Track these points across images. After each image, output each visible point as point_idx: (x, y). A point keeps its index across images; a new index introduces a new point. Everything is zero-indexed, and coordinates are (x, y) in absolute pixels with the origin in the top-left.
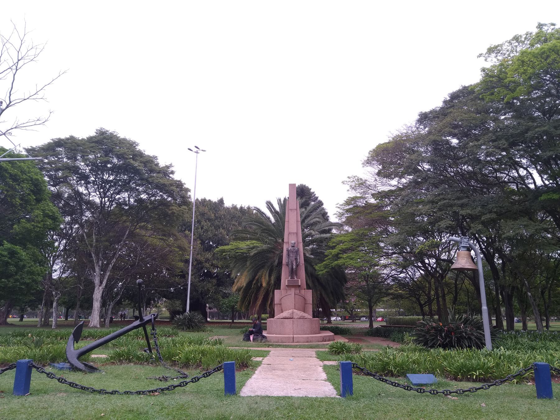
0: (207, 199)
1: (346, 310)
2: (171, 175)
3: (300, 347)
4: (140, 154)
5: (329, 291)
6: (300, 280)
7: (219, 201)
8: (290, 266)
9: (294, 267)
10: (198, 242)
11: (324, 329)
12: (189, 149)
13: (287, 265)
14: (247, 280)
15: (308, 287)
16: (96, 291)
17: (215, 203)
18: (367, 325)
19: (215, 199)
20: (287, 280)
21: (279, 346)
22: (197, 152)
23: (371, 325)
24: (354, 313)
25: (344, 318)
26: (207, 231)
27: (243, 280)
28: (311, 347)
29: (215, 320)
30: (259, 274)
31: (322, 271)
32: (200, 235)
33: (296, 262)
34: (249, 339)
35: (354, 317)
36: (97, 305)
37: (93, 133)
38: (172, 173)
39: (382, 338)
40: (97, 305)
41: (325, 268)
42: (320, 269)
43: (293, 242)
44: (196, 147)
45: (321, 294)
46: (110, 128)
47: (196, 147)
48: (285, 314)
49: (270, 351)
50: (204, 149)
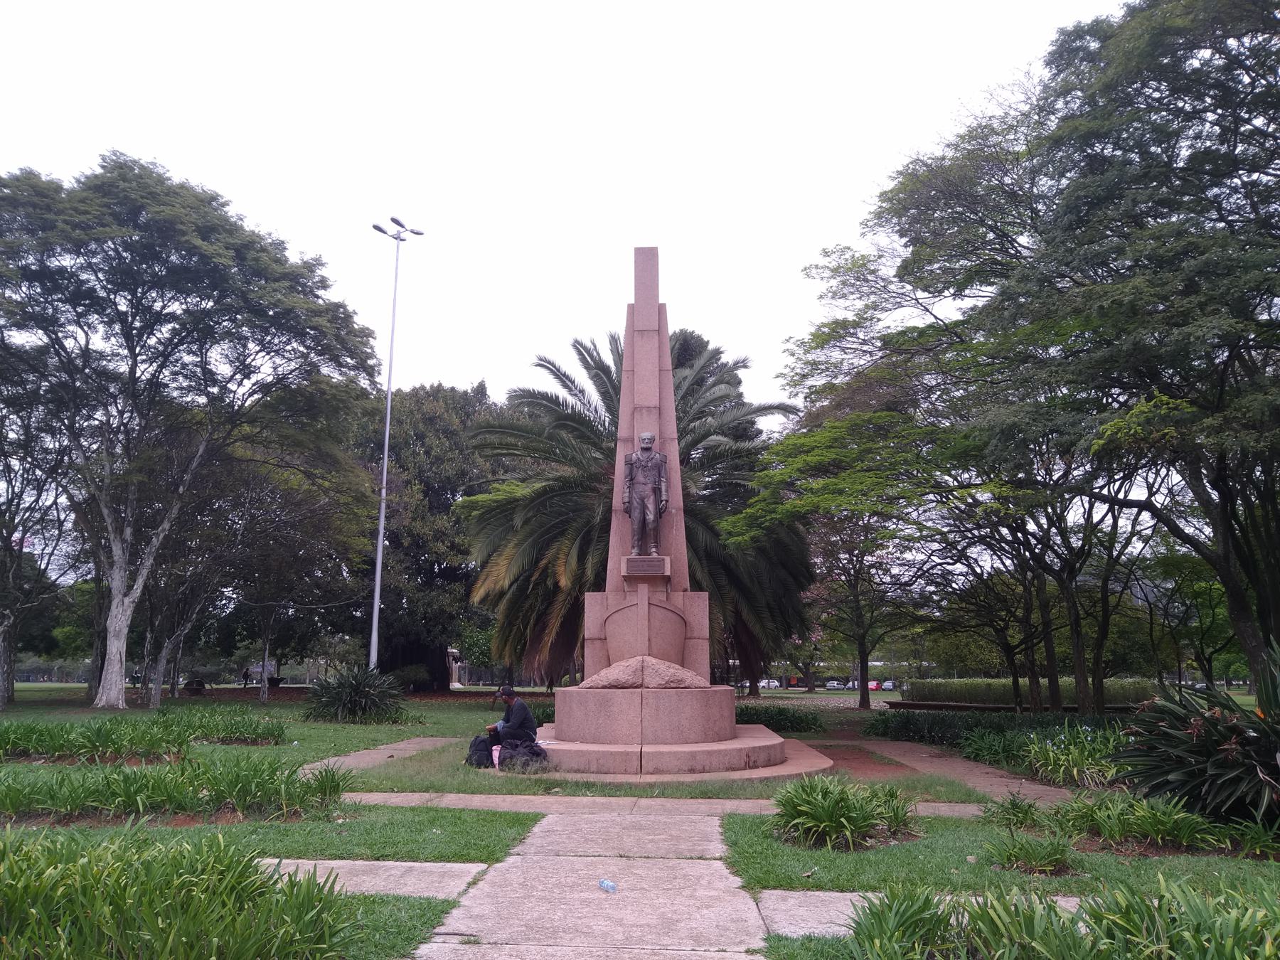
0: (447, 385)
1: (795, 664)
2: (320, 293)
3: (666, 791)
4: (232, 228)
5: (765, 588)
6: (667, 560)
7: (474, 390)
8: (636, 514)
9: (651, 517)
10: (415, 488)
11: (746, 717)
12: (377, 228)
13: (628, 511)
14: (515, 570)
15: (696, 586)
16: (114, 610)
17: (465, 393)
18: (853, 700)
19: (464, 384)
20: (624, 559)
21: (589, 787)
22: (397, 237)
23: (865, 702)
24: (812, 670)
25: (787, 683)
26: (439, 460)
27: (503, 569)
28: (706, 793)
29: (481, 688)
30: (550, 553)
31: (743, 534)
32: (421, 471)
33: (658, 501)
34: (486, 761)
35: (811, 680)
36: (116, 647)
37: (93, 167)
38: (324, 284)
39: (935, 750)
40: (116, 647)
41: (750, 526)
42: (734, 529)
43: (646, 435)
44: (395, 221)
45: (737, 613)
46: (141, 151)
47: (395, 221)
48: (617, 672)
49: (536, 818)
50: (417, 229)
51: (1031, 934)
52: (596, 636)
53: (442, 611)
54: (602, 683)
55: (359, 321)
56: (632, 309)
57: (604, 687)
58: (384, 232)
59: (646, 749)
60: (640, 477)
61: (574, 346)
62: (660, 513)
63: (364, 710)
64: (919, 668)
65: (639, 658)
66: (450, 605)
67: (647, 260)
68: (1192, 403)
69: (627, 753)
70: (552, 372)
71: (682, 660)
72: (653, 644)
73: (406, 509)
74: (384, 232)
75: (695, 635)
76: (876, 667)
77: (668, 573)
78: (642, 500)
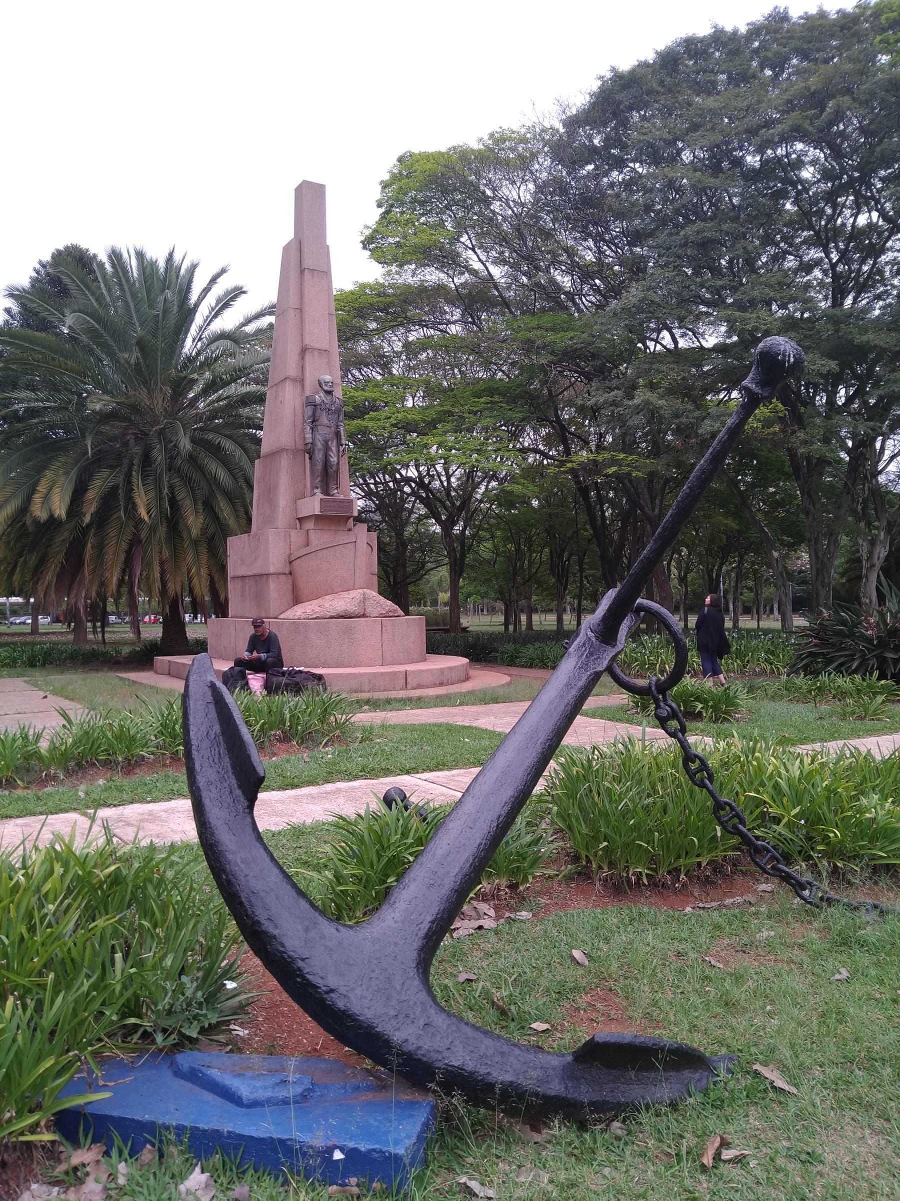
51: (39, 910)
52: (281, 571)
54: (329, 614)
57: (332, 617)
65: (361, 591)
68: (369, 495)
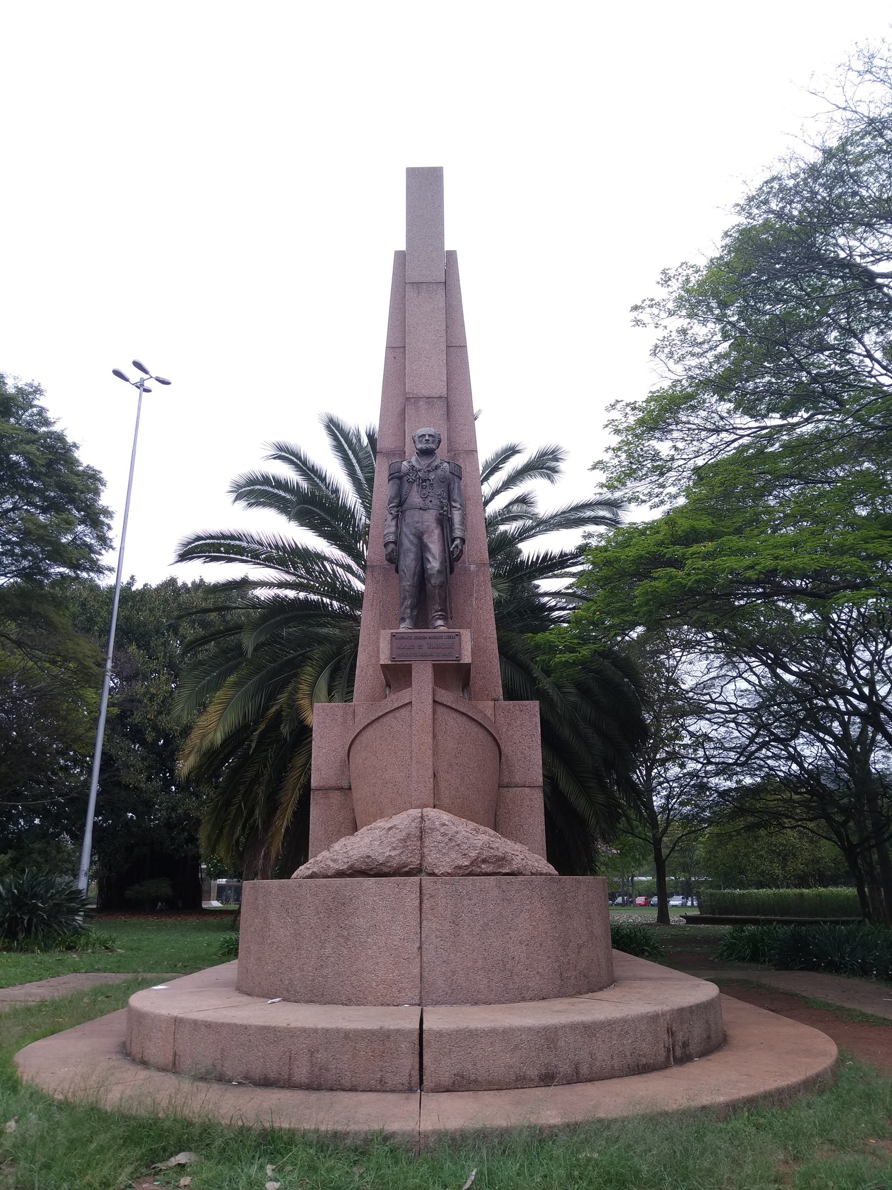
6: (466, 636)
8: (408, 561)
9: (434, 564)
12: (117, 373)
14: (232, 719)
18: (652, 915)
20: (385, 635)
22: (141, 386)
33: (447, 537)
44: (138, 365)
47: (138, 365)
48: (366, 843)
50: (163, 376)
52: (333, 782)
53: (187, 817)
54: (335, 866)
55: (85, 457)
56: (401, 259)
57: (340, 874)
58: (127, 380)
59: (438, 1020)
60: (415, 497)
61: (328, 428)
62: (451, 559)
63: (28, 931)
64: (688, 882)
65: (415, 812)
66: (197, 809)
67: (425, 190)
69: (384, 1036)
70: (291, 462)
71: (496, 821)
72: (442, 785)
73: (151, 700)
74: (127, 380)
75: (518, 778)
76: (642, 882)
77: (467, 659)
78: (419, 536)
